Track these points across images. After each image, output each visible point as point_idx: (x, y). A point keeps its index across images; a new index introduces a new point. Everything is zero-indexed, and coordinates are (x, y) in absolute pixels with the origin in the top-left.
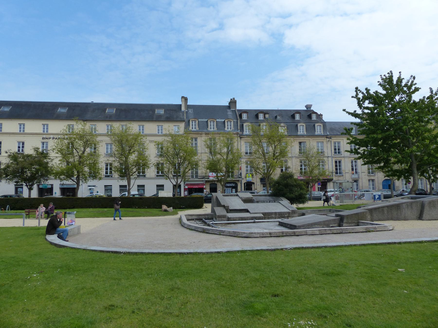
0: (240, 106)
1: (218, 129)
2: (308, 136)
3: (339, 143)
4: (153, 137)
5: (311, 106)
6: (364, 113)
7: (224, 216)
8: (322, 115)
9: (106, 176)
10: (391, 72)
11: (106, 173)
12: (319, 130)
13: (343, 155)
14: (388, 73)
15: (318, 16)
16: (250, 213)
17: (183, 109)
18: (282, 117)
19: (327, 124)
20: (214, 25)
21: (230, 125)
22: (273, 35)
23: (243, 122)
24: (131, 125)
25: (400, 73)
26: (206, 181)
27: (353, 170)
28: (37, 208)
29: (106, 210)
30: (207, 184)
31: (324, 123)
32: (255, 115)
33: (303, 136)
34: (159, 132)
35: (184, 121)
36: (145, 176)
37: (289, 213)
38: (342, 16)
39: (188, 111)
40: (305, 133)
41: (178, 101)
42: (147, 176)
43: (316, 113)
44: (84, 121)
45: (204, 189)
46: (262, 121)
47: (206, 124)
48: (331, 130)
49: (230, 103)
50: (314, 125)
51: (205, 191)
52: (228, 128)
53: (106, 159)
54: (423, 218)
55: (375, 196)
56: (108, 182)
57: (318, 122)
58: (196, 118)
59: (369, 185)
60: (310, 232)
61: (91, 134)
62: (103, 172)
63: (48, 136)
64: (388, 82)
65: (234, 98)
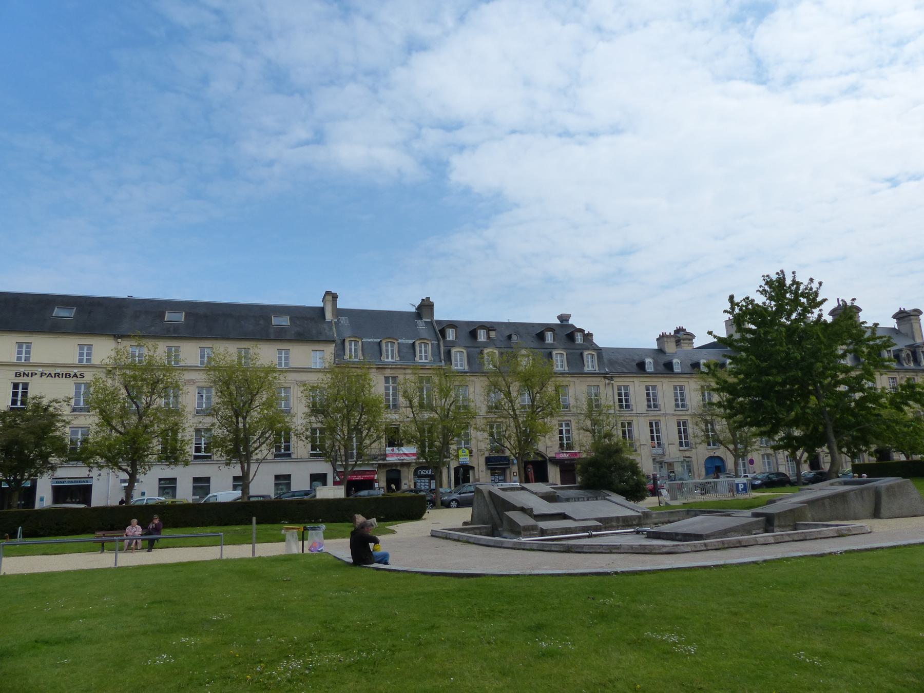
0: (440, 314)
1: (402, 358)
2: (573, 375)
3: (626, 387)
4: (299, 372)
5: (569, 316)
6: (743, 339)
7: (534, 528)
8: (592, 335)
9: (196, 457)
10: (782, 271)
11: (198, 449)
12: (590, 364)
13: (634, 412)
14: (777, 273)
15: (513, 132)
16: (575, 520)
17: (329, 316)
18: (521, 337)
19: (604, 354)
20: (302, 133)
21: (426, 352)
22: (425, 162)
23: (449, 346)
24: (257, 351)
25: (794, 273)
26: (380, 466)
27: (652, 438)
28: (124, 528)
29: (238, 528)
30: (380, 471)
31: (599, 350)
32: (471, 330)
33: (563, 374)
34: (280, 364)
35: (334, 341)
36: (289, 455)
37: (639, 517)
38: (560, 135)
39: (339, 321)
40: (567, 369)
41: (316, 302)
42: (294, 456)
43: (582, 331)
44: (116, 337)
45: (376, 481)
46: (486, 345)
47: (377, 348)
48: (612, 363)
49: (420, 308)
50: (582, 354)
51: (376, 485)
52: (421, 358)
53: (196, 420)
54: (882, 515)
55: (737, 485)
56: (201, 470)
57: (588, 349)
58: (357, 336)
59: (764, 463)
60: (761, 541)
61: (168, 369)
62: (190, 450)
63: (33, 370)
64: (777, 287)
65: (428, 299)
